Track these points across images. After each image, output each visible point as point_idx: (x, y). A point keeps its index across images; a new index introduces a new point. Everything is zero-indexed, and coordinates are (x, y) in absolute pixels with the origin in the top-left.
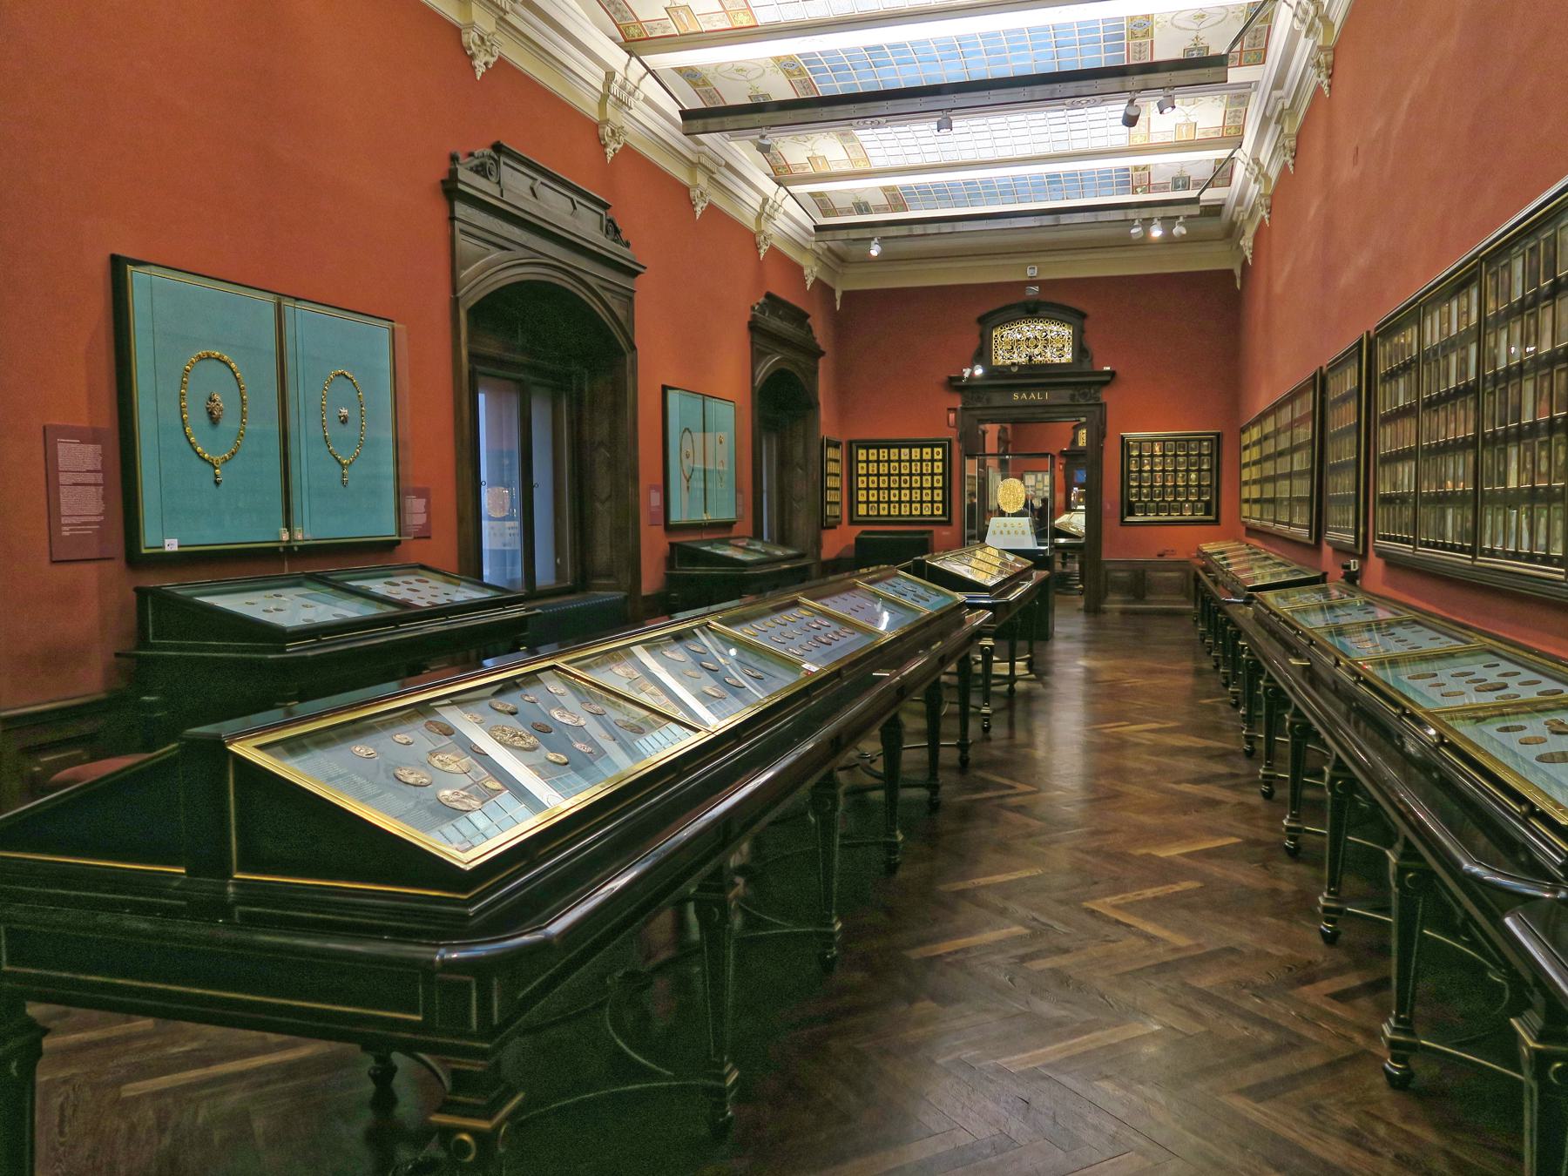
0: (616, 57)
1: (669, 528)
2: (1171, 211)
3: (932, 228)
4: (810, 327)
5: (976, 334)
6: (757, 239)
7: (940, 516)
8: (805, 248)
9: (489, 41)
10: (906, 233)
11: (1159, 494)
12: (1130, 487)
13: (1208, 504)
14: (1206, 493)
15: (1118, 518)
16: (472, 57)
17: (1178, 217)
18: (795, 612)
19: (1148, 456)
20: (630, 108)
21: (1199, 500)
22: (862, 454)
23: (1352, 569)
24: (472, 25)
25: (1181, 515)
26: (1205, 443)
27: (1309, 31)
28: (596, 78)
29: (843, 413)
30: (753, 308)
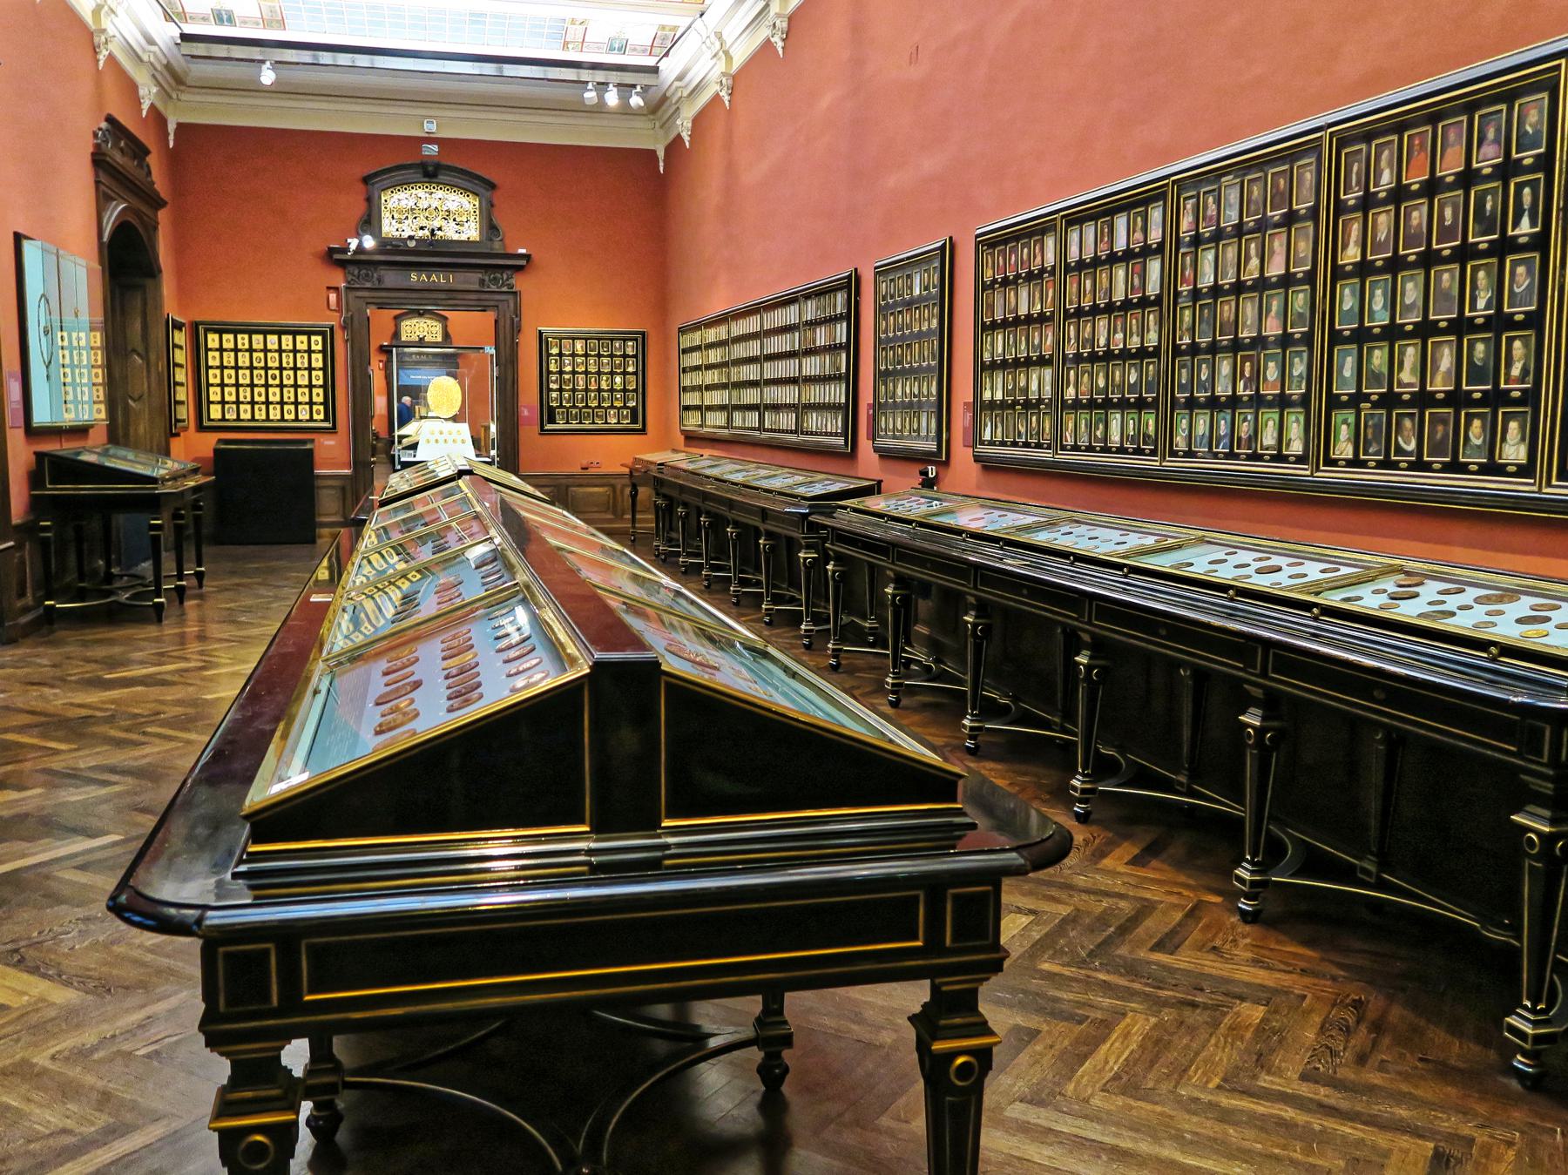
1: (32, 432)
2: (628, 78)
3: (220, 50)
4: (148, 166)
5: (361, 198)
7: (322, 421)
8: (141, 61)
10: (309, 60)
12: (550, 390)
13: (634, 410)
15: (537, 428)
17: (634, 86)
19: (569, 355)
21: (625, 407)
22: (213, 340)
23: (930, 476)
25: (606, 423)
26: (630, 343)
30: (95, 135)
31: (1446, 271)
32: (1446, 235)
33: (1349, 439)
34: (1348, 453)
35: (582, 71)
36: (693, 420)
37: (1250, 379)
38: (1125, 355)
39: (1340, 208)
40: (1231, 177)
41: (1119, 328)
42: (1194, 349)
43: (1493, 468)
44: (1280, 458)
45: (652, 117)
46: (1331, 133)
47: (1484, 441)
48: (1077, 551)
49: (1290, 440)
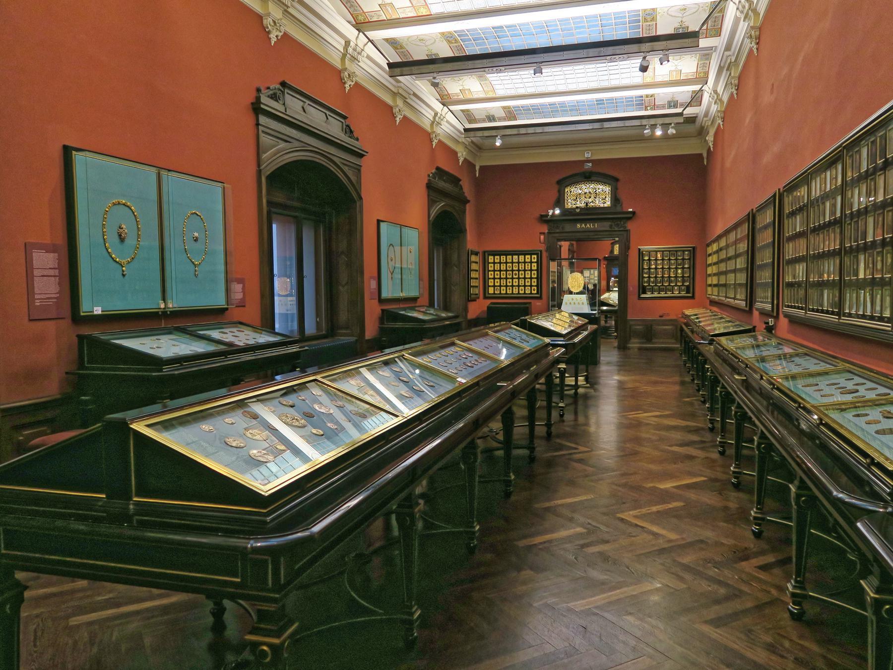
0: (351, 32)
1: (381, 301)
2: (667, 120)
3: (531, 130)
4: (461, 186)
5: (556, 190)
6: (431, 136)
7: (535, 294)
8: (459, 142)
9: (278, 23)
10: (516, 133)
11: (660, 282)
12: (644, 278)
13: (688, 287)
14: (687, 281)
15: (637, 295)
16: (269, 33)
17: (671, 124)
18: (453, 349)
19: (654, 260)
20: (359, 62)
21: (683, 285)
22: (491, 259)
23: (770, 324)
24: (269, 14)
25: (673, 293)
26: (686, 253)
27: (745, 18)
28: (339, 44)
30: (429, 176)
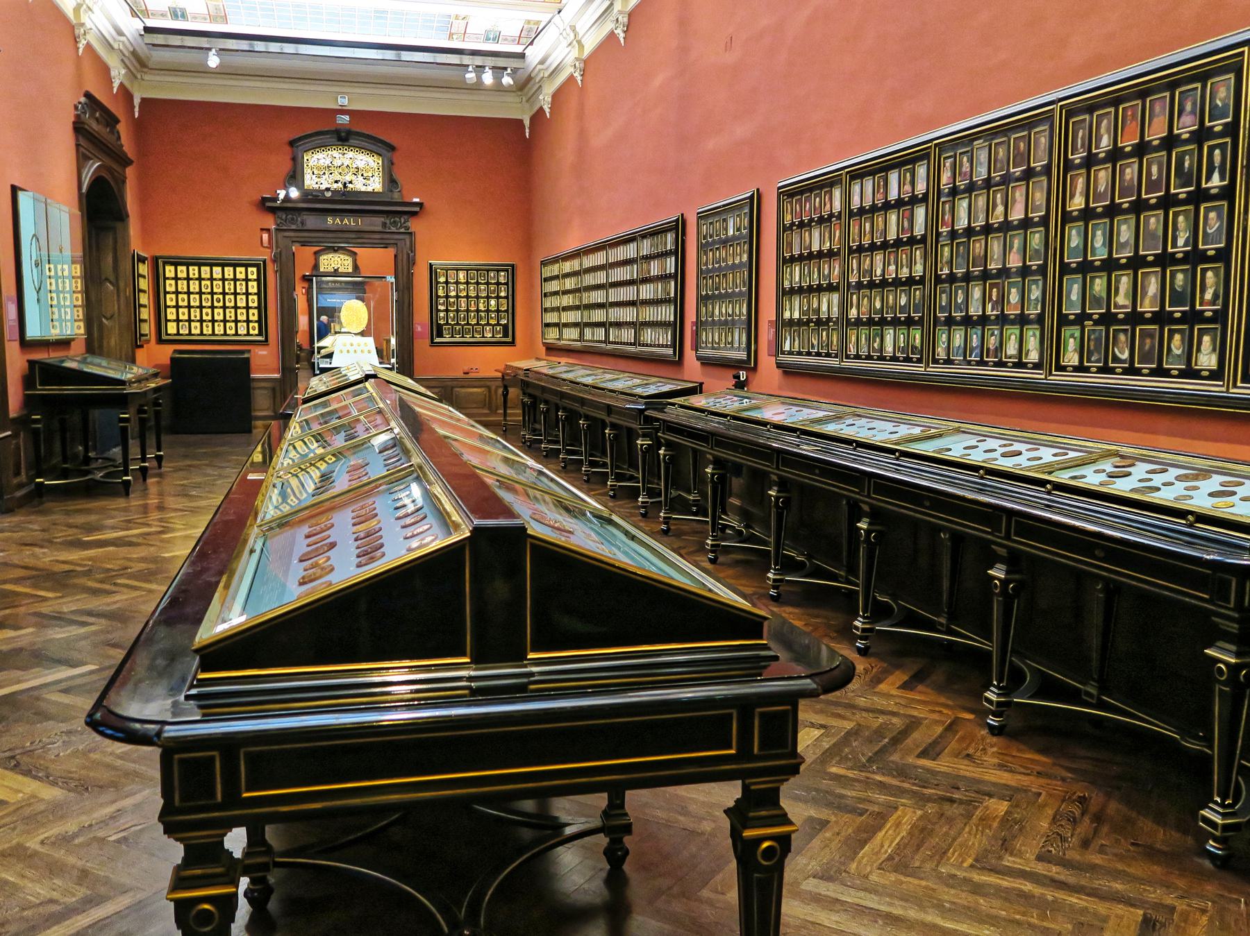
1: (26, 344)
2: (501, 62)
3: (176, 40)
4: (118, 132)
5: (288, 157)
7: (257, 335)
8: (113, 48)
10: (247, 48)
12: (438, 311)
13: (505, 327)
15: (428, 341)
17: (505, 69)
19: (454, 283)
21: (498, 324)
22: (170, 271)
23: (742, 379)
25: (483, 337)
26: (502, 274)
29: (146, 232)
30: (76, 108)
31: (1153, 216)
32: (1152, 187)
33: (1075, 350)
34: (1075, 361)
35: (464, 56)
36: (552, 335)
37: (996, 302)
38: (897, 282)
39: (1068, 166)
40: (981, 141)
41: (892, 261)
42: (952, 278)
43: (1190, 373)
44: (1020, 365)
45: (519, 93)
46: (1061, 106)
47: (1183, 351)
48: (859, 439)
49: (1028, 350)
